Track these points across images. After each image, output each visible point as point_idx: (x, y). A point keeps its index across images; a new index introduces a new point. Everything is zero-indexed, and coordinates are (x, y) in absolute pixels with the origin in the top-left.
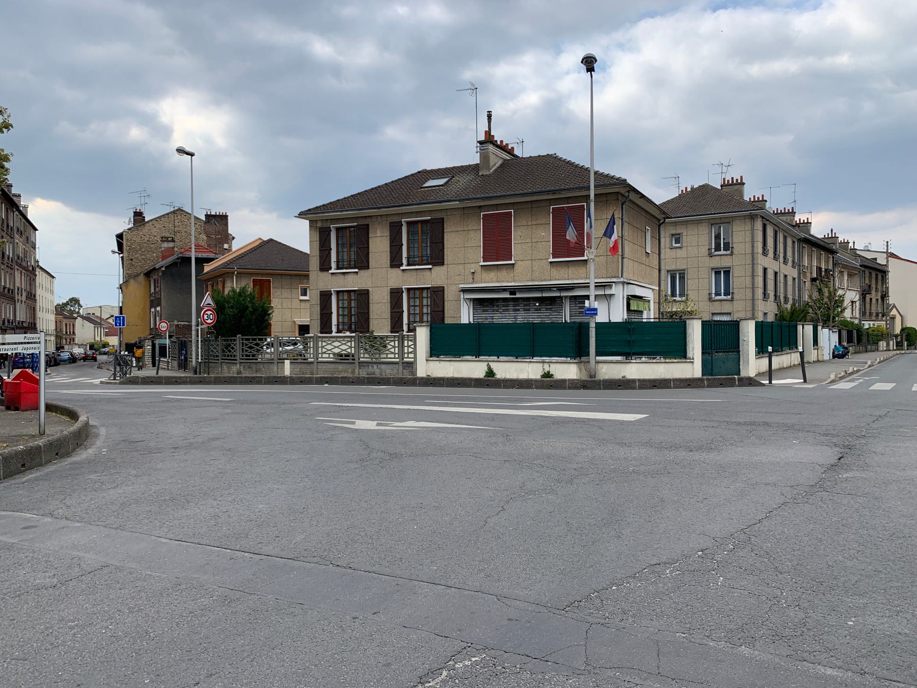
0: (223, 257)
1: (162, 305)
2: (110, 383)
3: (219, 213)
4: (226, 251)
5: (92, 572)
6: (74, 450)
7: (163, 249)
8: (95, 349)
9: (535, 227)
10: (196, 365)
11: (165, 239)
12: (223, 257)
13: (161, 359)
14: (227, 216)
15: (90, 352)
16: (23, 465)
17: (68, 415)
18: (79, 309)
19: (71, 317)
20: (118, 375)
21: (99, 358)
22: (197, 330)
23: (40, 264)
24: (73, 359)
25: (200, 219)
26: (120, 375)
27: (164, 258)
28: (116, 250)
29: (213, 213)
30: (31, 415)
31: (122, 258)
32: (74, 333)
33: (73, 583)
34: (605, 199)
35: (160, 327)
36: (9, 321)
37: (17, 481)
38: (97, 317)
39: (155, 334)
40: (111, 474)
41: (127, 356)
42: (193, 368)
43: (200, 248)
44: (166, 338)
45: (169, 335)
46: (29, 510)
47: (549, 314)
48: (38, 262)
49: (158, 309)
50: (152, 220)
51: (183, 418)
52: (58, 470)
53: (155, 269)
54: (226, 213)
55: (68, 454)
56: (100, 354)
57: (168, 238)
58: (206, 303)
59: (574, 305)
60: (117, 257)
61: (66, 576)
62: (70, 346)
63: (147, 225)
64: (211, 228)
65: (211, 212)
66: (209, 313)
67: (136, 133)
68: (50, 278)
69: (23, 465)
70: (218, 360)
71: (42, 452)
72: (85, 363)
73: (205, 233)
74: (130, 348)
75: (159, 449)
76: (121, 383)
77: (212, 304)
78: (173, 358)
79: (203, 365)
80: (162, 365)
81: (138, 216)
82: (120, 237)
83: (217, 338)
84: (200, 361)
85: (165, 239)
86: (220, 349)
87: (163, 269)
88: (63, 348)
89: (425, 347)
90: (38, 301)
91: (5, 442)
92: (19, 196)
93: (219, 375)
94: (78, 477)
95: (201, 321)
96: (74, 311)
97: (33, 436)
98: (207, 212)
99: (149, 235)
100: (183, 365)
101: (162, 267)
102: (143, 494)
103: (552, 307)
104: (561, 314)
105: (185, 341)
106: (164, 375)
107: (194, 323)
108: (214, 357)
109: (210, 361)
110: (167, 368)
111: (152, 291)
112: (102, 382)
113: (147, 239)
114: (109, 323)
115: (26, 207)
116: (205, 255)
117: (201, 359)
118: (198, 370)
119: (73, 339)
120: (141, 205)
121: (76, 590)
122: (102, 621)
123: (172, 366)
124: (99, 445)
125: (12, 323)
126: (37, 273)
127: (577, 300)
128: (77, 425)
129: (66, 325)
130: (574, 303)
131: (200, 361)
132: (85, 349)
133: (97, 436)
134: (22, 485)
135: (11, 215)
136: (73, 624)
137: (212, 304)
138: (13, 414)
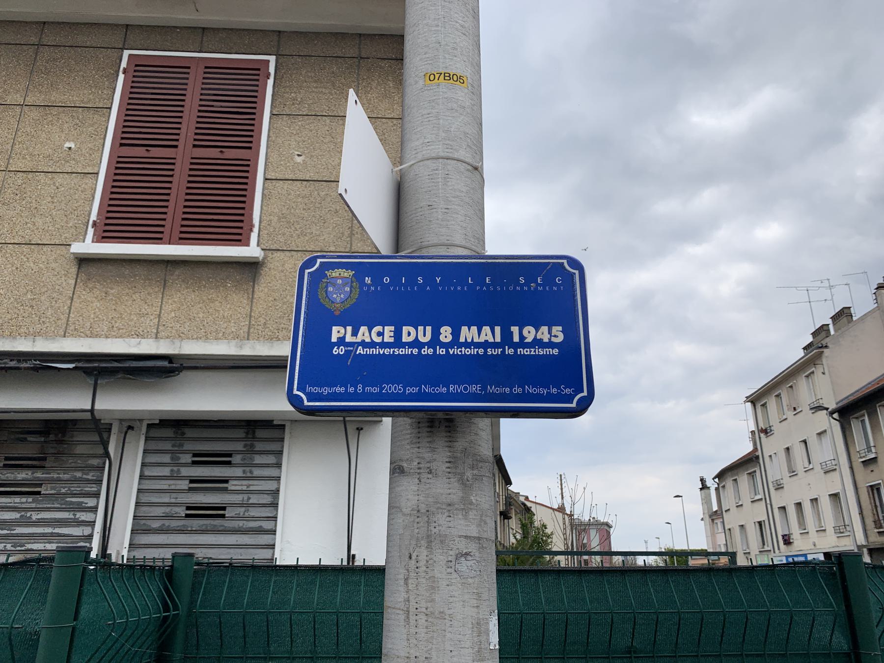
9: (35, 114)
34: (353, 52)
47: (15, 515)
59: (166, 471)
89: (806, 509)
103: (39, 474)
104: (83, 516)
127: (188, 446)
130: (166, 458)
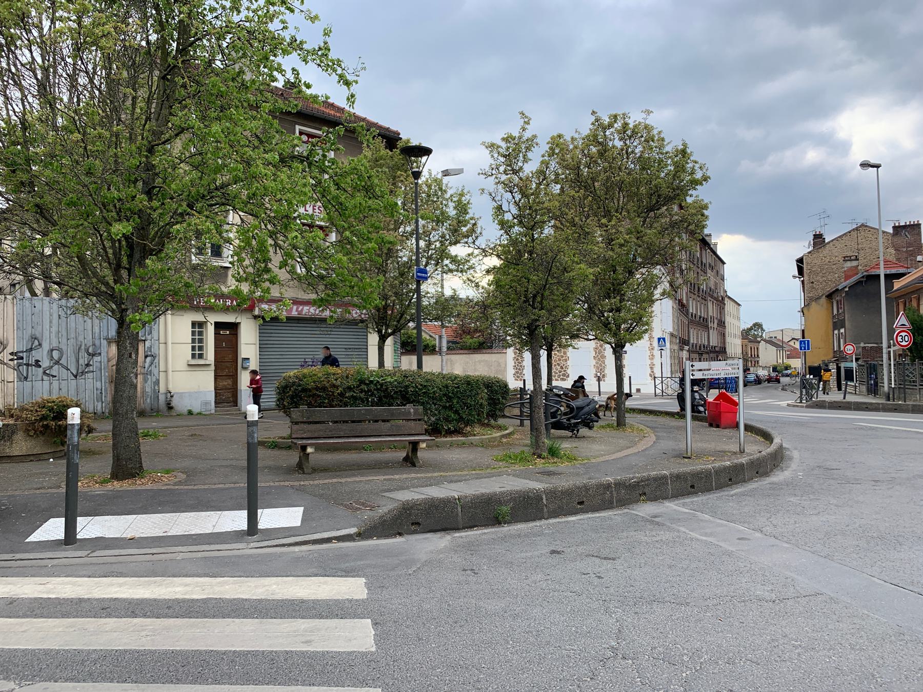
0: (916, 271)
1: (846, 327)
2: (797, 406)
3: (910, 222)
4: (919, 263)
5: (807, 596)
6: (772, 470)
7: (846, 269)
8: (777, 371)
10: (889, 389)
11: (847, 259)
12: (916, 271)
13: (849, 383)
14: (920, 224)
15: (773, 374)
16: (730, 480)
17: (762, 436)
18: (762, 333)
19: (755, 341)
20: (804, 398)
21: (782, 379)
22: (889, 352)
23: (728, 294)
24: (758, 381)
25: (887, 233)
26: (806, 398)
27: (847, 278)
28: (797, 274)
29: (902, 224)
30: (730, 432)
31: (803, 282)
32: (758, 356)
33: (790, 603)
35: (846, 350)
36: (704, 346)
37: (726, 493)
38: (779, 340)
39: (840, 357)
40: (811, 500)
41: (812, 379)
42: (886, 393)
43: (889, 263)
44: (852, 361)
45: (856, 358)
46: (741, 523)
48: (726, 292)
49: (842, 331)
50: (832, 241)
51: (880, 449)
52: (760, 488)
53: (837, 290)
54: (918, 221)
55: (766, 474)
56: (783, 376)
57: (850, 257)
58: (899, 324)
60: (798, 282)
61: (783, 594)
62: (755, 368)
63: (828, 246)
64: (900, 241)
65: (899, 223)
66: (903, 334)
67: (812, 156)
68: (736, 306)
69: (730, 480)
70: (916, 386)
71: (746, 470)
72: (769, 384)
73: (894, 246)
74: (815, 371)
75: (857, 480)
76: (807, 407)
77: (907, 324)
78: (861, 383)
79: (897, 391)
80: (849, 389)
81: (818, 239)
82: (800, 261)
83: (913, 361)
84: (893, 386)
85: (847, 259)
86: (917, 373)
87: (847, 289)
88: (749, 370)
90: (727, 327)
91: (713, 456)
92: (710, 235)
93: (918, 403)
94: (779, 498)
95: (894, 343)
96: (758, 335)
97: (735, 453)
98: (895, 224)
99: (830, 256)
100: (874, 389)
101: (846, 287)
102: (848, 526)
105: (874, 364)
106: (853, 401)
107: (885, 345)
108: (910, 382)
109: (907, 387)
110: (854, 392)
111: (835, 312)
112: (788, 405)
113: (828, 260)
114: (790, 346)
115: (716, 245)
116: (893, 271)
117: (895, 384)
118: (891, 396)
119: (758, 362)
120: (821, 226)
121: (794, 610)
122: (824, 649)
123: (859, 390)
124: (794, 468)
125: (707, 347)
126: (726, 302)
128: (773, 448)
129: (751, 349)
131: (893, 386)
132: (769, 371)
133: (791, 459)
134: (731, 498)
135: (704, 252)
136: (796, 643)
137: (907, 324)
138: (715, 431)
